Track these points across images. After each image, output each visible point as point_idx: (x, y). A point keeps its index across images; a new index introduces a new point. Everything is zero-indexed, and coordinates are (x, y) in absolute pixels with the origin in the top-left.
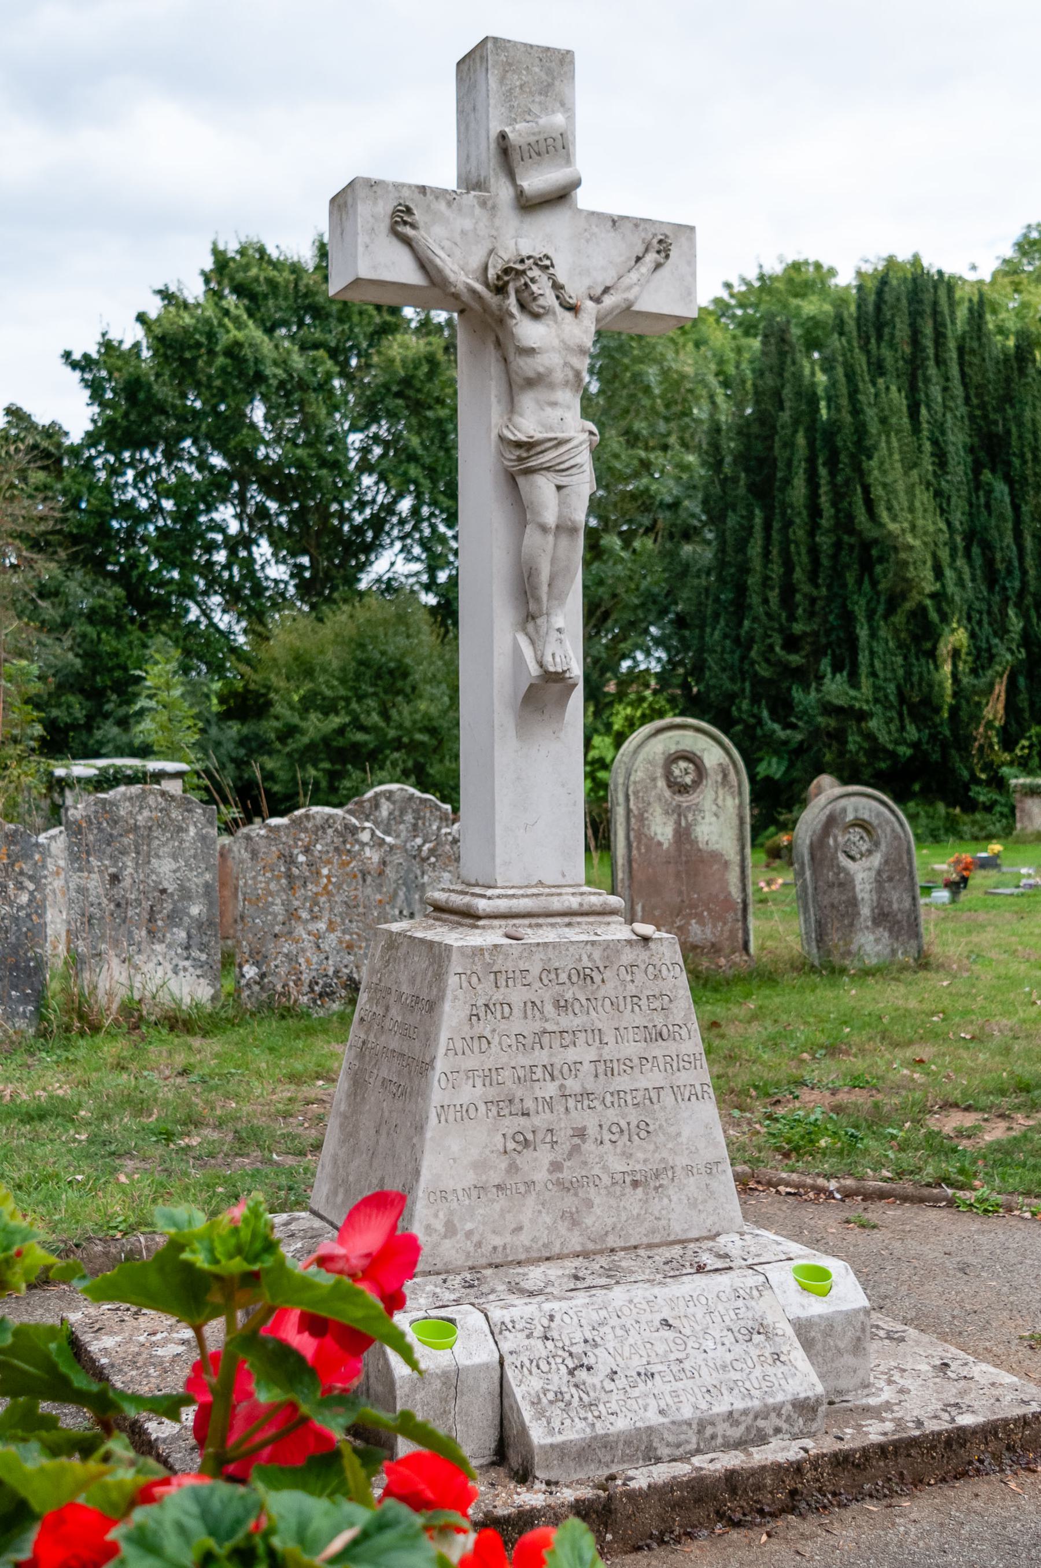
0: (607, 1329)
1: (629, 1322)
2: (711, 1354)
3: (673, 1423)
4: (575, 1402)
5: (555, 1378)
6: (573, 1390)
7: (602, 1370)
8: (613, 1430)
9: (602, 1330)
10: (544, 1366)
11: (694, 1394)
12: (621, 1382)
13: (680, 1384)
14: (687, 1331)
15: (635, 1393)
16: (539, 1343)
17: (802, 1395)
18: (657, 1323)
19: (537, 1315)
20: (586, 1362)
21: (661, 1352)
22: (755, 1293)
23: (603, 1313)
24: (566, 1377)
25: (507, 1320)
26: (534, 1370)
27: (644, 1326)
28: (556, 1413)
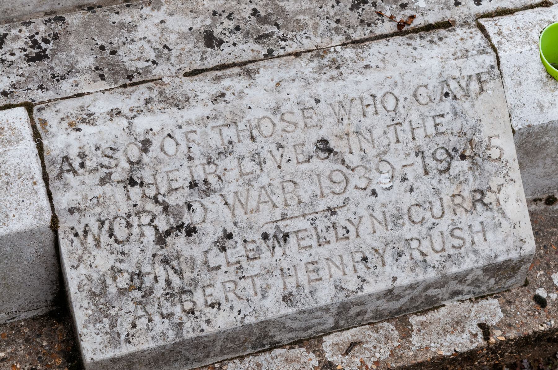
0: (230, 162)
1: (265, 146)
2: (382, 197)
3: (302, 312)
4: (160, 289)
5: (134, 249)
6: (160, 270)
7: (211, 232)
8: (208, 330)
9: (223, 163)
10: (121, 232)
11: (342, 266)
12: (236, 251)
13: (324, 251)
14: (353, 160)
15: (255, 268)
16: (119, 191)
17: (501, 259)
18: (310, 148)
19: (124, 139)
20: (187, 219)
21: (305, 198)
22: (474, 86)
23: (229, 133)
24: (152, 248)
25: (73, 153)
26: (105, 238)
27: (289, 152)
28: (126, 309)
